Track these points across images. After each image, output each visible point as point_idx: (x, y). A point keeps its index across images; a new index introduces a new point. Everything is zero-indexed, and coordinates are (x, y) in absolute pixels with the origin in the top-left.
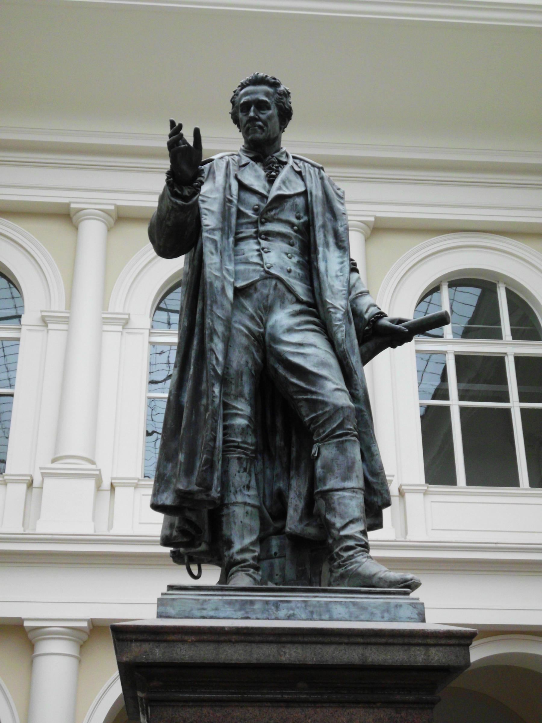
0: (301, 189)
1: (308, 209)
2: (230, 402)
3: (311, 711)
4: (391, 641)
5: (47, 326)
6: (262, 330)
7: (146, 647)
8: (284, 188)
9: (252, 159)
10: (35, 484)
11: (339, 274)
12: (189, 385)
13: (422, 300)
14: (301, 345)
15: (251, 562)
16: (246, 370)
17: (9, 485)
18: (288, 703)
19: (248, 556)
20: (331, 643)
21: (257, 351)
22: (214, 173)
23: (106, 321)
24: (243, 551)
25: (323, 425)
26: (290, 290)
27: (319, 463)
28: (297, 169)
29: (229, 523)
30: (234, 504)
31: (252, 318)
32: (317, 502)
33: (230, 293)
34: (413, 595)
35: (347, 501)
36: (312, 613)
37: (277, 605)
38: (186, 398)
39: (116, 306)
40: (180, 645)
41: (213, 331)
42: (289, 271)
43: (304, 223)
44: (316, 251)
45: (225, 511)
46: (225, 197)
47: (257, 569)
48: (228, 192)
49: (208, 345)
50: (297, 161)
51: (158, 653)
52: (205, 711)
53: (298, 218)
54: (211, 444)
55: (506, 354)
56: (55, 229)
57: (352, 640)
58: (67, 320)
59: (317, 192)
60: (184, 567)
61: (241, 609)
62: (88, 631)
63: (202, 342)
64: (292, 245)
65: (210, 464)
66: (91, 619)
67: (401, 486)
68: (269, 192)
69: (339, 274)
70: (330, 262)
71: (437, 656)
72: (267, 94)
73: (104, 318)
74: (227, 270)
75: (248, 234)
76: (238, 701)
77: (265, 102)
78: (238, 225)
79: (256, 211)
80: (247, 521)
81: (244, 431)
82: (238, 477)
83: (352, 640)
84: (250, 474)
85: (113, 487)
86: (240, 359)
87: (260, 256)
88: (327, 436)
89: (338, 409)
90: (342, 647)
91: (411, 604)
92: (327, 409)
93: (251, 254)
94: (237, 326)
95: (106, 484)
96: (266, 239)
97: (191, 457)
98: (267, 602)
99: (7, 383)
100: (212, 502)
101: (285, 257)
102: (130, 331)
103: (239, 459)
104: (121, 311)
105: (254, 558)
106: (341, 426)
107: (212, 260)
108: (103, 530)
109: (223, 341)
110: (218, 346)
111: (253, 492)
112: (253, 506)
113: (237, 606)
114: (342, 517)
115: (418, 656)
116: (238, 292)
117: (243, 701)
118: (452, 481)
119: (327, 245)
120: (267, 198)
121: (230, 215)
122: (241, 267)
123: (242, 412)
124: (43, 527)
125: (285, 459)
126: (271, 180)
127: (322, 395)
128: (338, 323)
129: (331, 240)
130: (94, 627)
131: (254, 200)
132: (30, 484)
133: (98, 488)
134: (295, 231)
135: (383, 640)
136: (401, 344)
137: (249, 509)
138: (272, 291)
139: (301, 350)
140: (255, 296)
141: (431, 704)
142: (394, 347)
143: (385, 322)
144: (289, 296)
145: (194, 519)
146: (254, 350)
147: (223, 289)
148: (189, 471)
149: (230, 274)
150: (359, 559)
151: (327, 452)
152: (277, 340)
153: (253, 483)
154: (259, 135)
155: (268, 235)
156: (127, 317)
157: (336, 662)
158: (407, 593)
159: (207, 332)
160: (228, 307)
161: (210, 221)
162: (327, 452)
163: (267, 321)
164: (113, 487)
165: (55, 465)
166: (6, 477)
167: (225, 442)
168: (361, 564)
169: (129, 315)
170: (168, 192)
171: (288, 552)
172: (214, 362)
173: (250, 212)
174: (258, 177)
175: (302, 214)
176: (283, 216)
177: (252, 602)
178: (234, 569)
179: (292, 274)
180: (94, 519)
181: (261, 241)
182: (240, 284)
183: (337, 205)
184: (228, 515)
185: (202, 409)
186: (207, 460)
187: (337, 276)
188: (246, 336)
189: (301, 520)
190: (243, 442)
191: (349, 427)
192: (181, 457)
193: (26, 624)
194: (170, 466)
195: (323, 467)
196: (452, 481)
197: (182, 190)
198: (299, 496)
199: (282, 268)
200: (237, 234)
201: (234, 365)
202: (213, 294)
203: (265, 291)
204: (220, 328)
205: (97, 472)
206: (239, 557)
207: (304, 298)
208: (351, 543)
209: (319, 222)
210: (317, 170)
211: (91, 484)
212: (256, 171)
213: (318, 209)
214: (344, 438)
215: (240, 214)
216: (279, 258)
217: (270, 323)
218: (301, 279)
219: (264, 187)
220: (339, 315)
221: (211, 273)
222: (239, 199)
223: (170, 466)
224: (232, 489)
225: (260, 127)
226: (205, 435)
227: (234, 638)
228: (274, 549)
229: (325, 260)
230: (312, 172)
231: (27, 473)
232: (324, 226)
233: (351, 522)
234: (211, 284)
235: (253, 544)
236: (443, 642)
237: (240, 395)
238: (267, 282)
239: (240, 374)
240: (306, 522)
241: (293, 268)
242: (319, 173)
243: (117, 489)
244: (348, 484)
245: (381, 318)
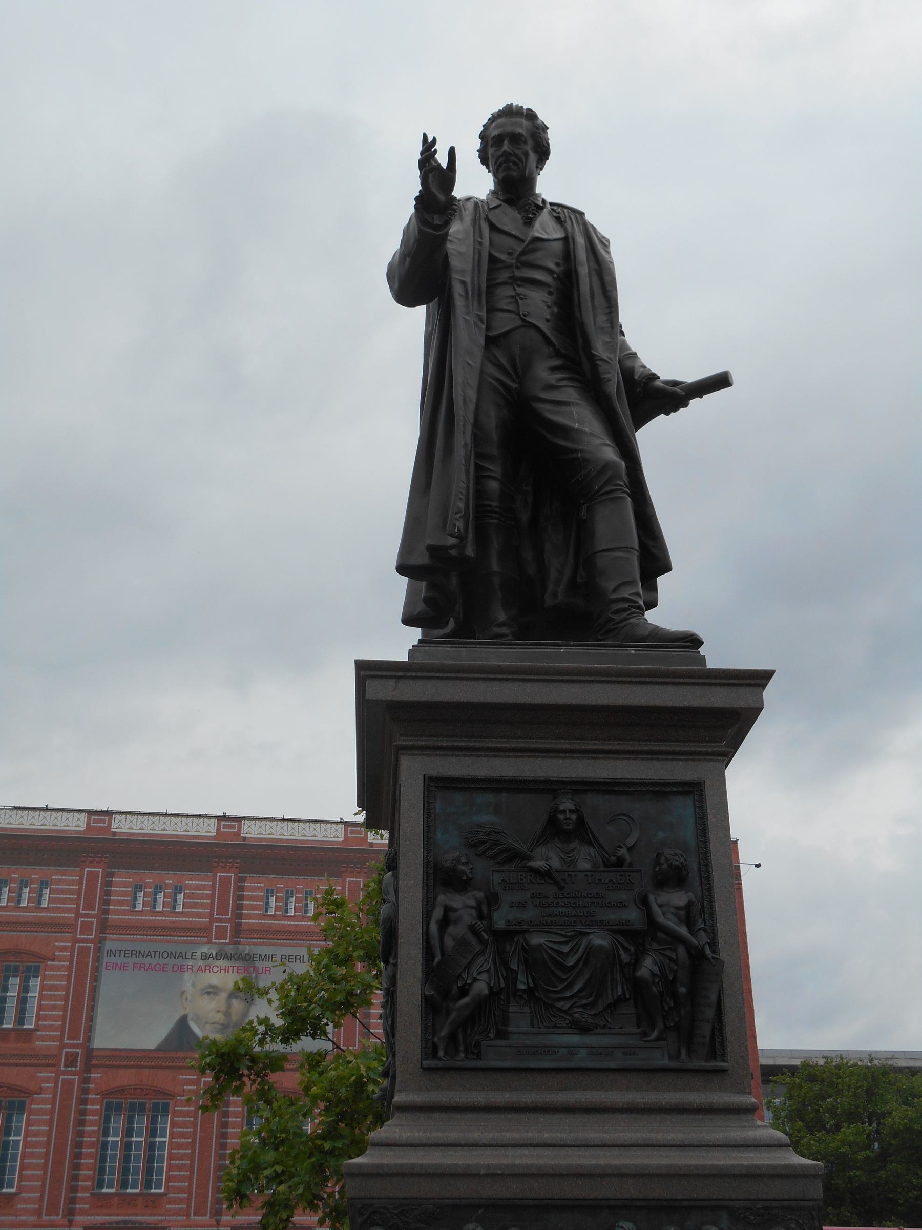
50: (555, 208)
136: (675, 409)
142: (668, 414)
143: (658, 383)
173: (503, 257)
230: (573, 217)
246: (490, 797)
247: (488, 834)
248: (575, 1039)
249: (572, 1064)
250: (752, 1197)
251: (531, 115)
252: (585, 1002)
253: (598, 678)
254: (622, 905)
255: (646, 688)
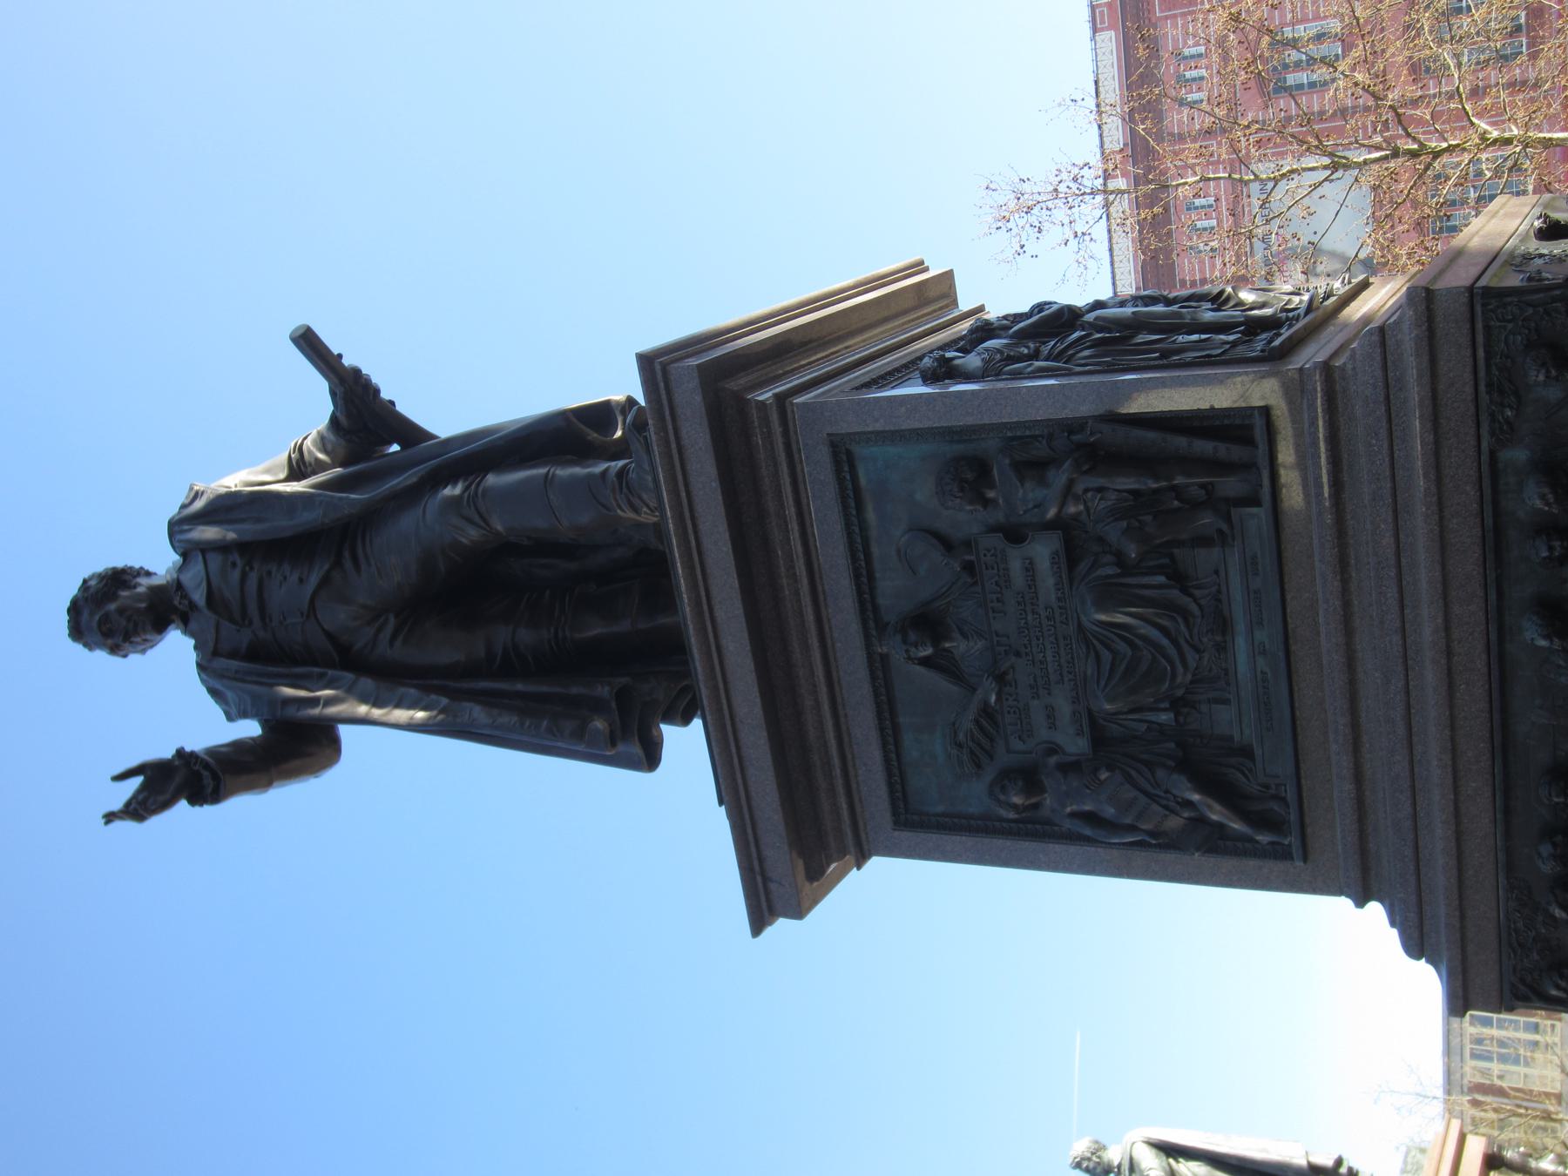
246: (908, 739)
247: (960, 746)
248: (1241, 643)
249: (1281, 654)
250: (1472, 409)
251: (75, 609)
252: (1183, 627)
253: (707, 615)
254: (1030, 568)
255: (707, 543)
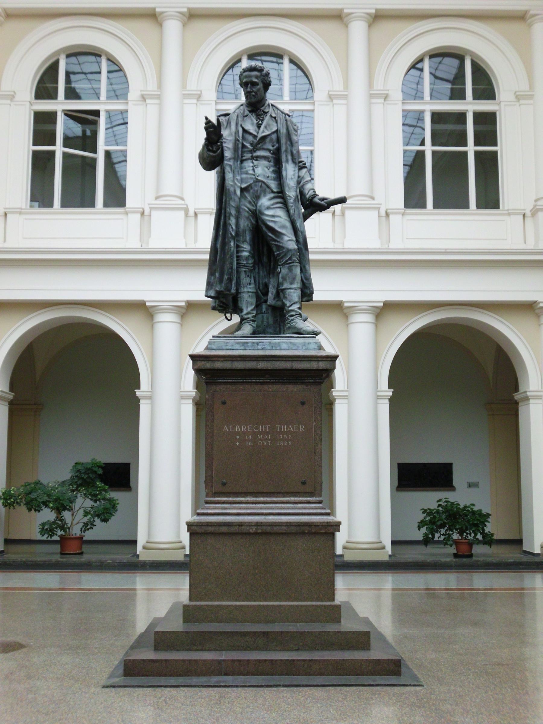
0: (275, 129)
1: (278, 140)
2: (240, 245)
3: (271, 386)
4: (303, 359)
5: (145, 101)
6: (254, 208)
7: (203, 363)
8: (266, 131)
9: (250, 112)
10: (146, 213)
11: (293, 177)
12: (220, 239)
13: (406, 74)
14: (273, 216)
15: (252, 318)
16: (247, 228)
17: (130, 215)
18: (262, 383)
19: (250, 316)
20: (278, 361)
21: (253, 218)
22: (230, 123)
23: (186, 96)
24: (248, 313)
25: (282, 258)
26: (268, 187)
27: (280, 276)
28: (274, 115)
29: (241, 301)
30: (243, 292)
31: (250, 202)
32: (280, 293)
33: (238, 192)
34: (317, 337)
35: (292, 294)
36: (272, 347)
37: (258, 344)
38: (219, 246)
39: (192, 86)
40: (217, 362)
41: (230, 214)
42: (268, 177)
43: (276, 149)
44: (282, 165)
45: (239, 296)
46: (236, 138)
47: (254, 321)
48: (237, 135)
49: (228, 222)
51: (208, 365)
52: (228, 386)
53: (273, 146)
54: (230, 270)
55: (467, 110)
56: (145, 26)
57: (287, 359)
58: (159, 97)
59: (283, 131)
60: (223, 314)
61: (243, 346)
62: (185, 307)
63: (225, 217)
64: (270, 162)
65: (230, 280)
66: (187, 301)
67: (387, 210)
68: (258, 133)
69: (293, 177)
70: (290, 171)
71: (322, 365)
72: (257, 77)
73: (184, 94)
74: (237, 179)
75: (248, 157)
76: (241, 382)
77: (256, 82)
78: (243, 152)
79: (251, 144)
80: (249, 300)
81: (247, 258)
82: (245, 280)
83: (287, 359)
84: (251, 278)
85: (196, 214)
86: (244, 223)
87: (254, 170)
88: (284, 263)
89: (289, 250)
90: (283, 362)
91: (315, 342)
92: (284, 250)
93: (249, 169)
94: (243, 207)
95: (191, 213)
96: (256, 160)
97: (222, 274)
98: (254, 343)
99: (113, 81)
100: (232, 294)
101: (266, 169)
102: (203, 102)
103: (245, 271)
104: (195, 89)
105: (253, 317)
106: (290, 259)
107: (229, 176)
108: (192, 245)
109: (235, 218)
110: (233, 221)
111: (252, 286)
112: (252, 292)
113: (241, 344)
114: (290, 301)
115: (314, 365)
116: (242, 190)
117: (243, 382)
118: (423, 206)
119: (287, 161)
120: (257, 137)
121: (238, 148)
122: (244, 176)
123: (246, 249)
124: (154, 243)
125: (268, 268)
126: (259, 127)
127: (281, 243)
128: (291, 205)
129: (290, 158)
130: (189, 304)
131: (250, 138)
132: (143, 214)
133: (187, 215)
134: (272, 154)
135: (300, 359)
137: (250, 294)
138: (259, 188)
139: (273, 219)
140: (251, 191)
141: (321, 383)
143: (316, 200)
144: (268, 190)
145: (224, 301)
146: (251, 218)
147: (235, 191)
148: (221, 280)
149: (238, 181)
150: (296, 320)
151: (284, 271)
152: (262, 213)
153: (253, 281)
154: (253, 100)
155: (257, 158)
156: (199, 93)
157: (280, 368)
158: (315, 338)
159: (227, 215)
160: (237, 199)
161: (228, 154)
162: (284, 271)
163: (257, 203)
164: (196, 214)
165: (158, 202)
166: (127, 210)
167: (238, 263)
168: (297, 323)
169: (201, 91)
170: (206, 149)
171: (270, 311)
172: (231, 230)
173: (248, 145)
174: (253, 124)
175: (275, 144)
176: (265, 147)
177: (247, 343)
178: (244, 322)
179: (270, 178)
180: (185, 237)
181: (254, 161)
182: (244, 186)
183: (294, 138)
184: (240, 297)
185: (226, 251)
186: (228, 278)
187: (292, 178)
188: (247, 212)
189: (274, 299)
190: (247, 264)
191: (294, 259)
192: (217, 275)
193: (147, 304)
194: (213, 278)
195: (282, 278)
196: (423, 206)
197: (212, 147)
198: (274, 287)
199: (264, 176)
200: (242, 157)
201: (242, 226)
202: (230, 195)
203: (256, 189)
204: (233, 212)
205: (185, 206)
206: (246, 317)
207: (275, 190)
208: (293, 313)
209: (283, 149)
210: (284, 115)
211: (182, 213)
212: (252, 120)
213: (283, 141)
214: (292, 264)
215: (243, 146)
216: (262, 170)
217: (259, 204)
218: (275, 179)
219: (256, 131)
220: (292, 201)
221: (229, 184)
222: (243, 138)
223: (213, 278)
224: (242, 285)
225: (253, 95)
226: (227, 267)
227: (239, 359)
228: (264, 310)
229: (286, 170)
231: (140, 206)
232: (286, 151)
233: (294, 303)
234: (229, 189)
235: (252, 310)
236: (325, 359)
237: (245, 241)
238: (257, 183)
239: (244, 231)
240: (277, 299)
241: (270, 175)
242: (285, 117)
243: (199, 216)
244: (293, 286)
245: (314, 197)
